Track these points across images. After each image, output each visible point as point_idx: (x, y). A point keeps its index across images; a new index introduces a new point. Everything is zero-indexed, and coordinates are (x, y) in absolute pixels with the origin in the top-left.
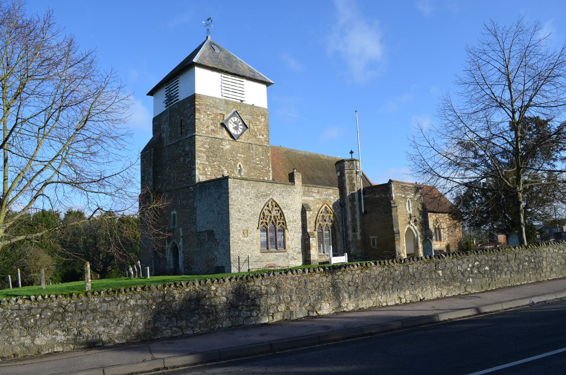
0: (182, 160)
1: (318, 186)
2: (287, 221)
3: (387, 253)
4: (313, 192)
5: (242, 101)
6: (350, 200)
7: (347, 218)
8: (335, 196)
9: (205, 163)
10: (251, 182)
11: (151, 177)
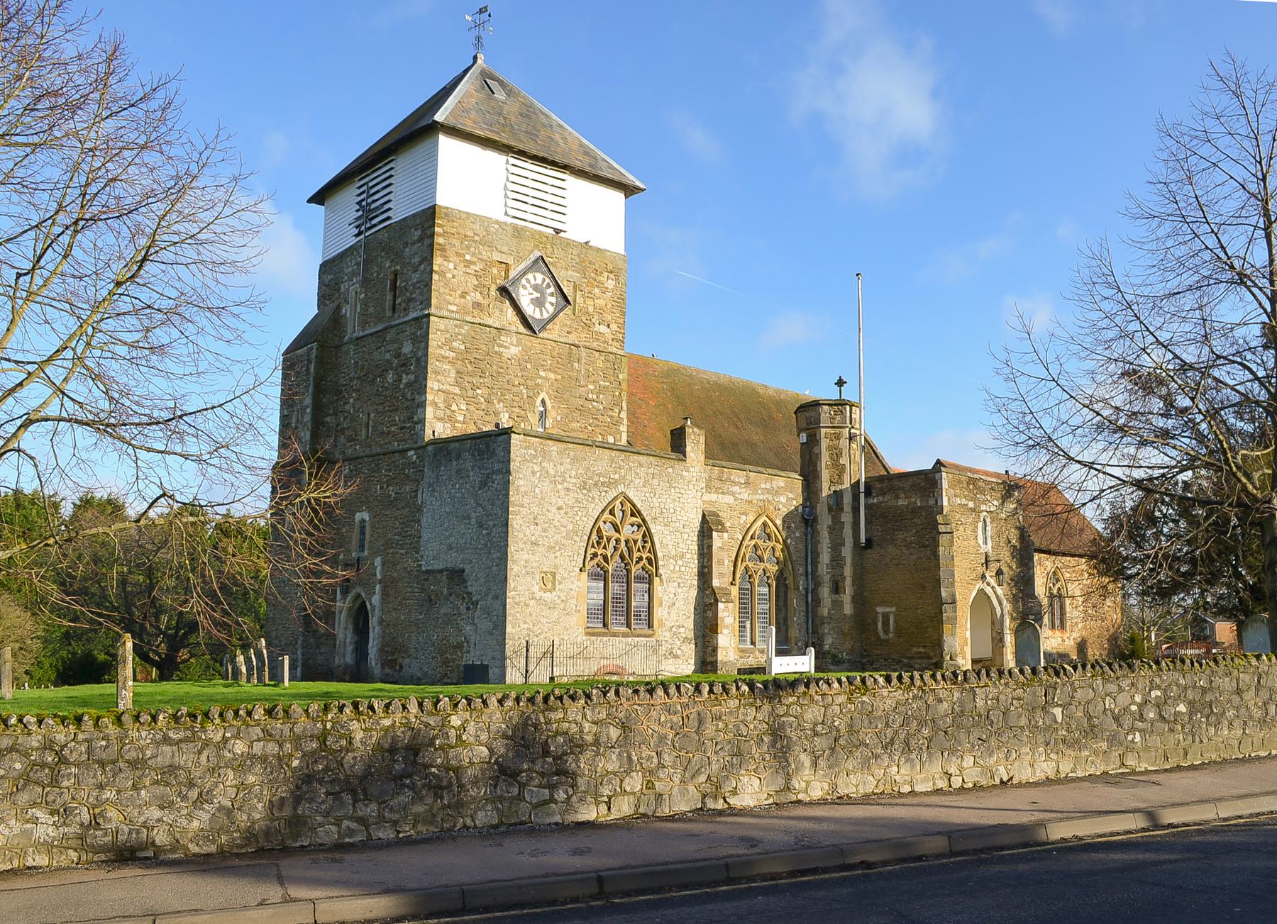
0: (390, 377)
2: (660, 555)
3: (920, 653)
5: (558, 231)
6: (830, 509)
9: (451, 388)
10: (570, 446)
11: (307, 418)
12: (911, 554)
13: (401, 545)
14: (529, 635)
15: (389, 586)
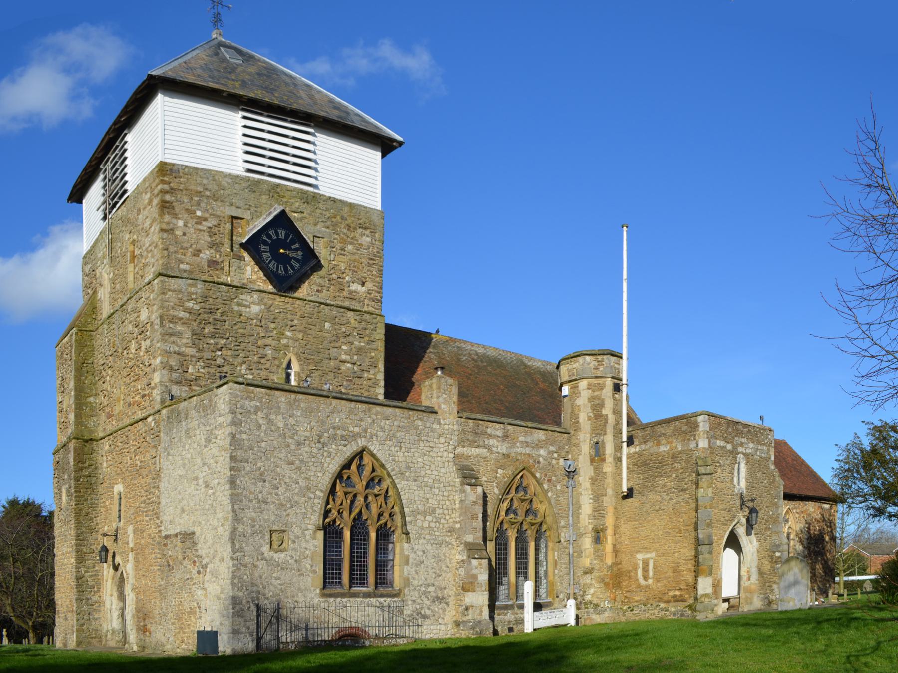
0: (133, 346)
1: (506, 420)
3: (676, 596)
4: (490, 436)
7: (580, 507)
8: (552, 448)
10: (301, 396)
12: (671, 499)
13: (146, 512)
14: (258, 599)
15: (138, 551)
